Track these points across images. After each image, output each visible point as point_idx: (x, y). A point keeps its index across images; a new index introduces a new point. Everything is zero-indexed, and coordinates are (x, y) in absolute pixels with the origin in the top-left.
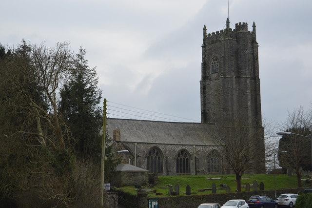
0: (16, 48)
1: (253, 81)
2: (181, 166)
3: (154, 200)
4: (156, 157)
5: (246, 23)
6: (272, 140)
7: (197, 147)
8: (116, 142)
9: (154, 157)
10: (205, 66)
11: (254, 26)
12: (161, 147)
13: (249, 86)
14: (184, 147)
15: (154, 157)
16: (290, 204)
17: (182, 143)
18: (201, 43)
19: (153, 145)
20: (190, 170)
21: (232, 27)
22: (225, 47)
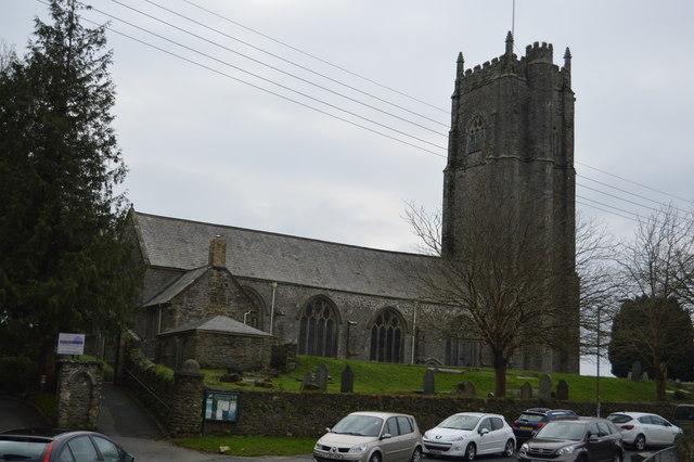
1: (560, 173)
2: (382, 345)
3: (226, 395)
4: (322, 321)
5: (551, 45)
6: (612, 376)
8: (214, 268)
10: (456, 137)
11: (568, 56)
12: (335, 298)
13: (550, 179)
14: (392, 303)
16: (637, 441)
17: (387, 294)
18: (451, 90)
19: (319, 292)
20: (403, 357)
21: (520, 52)
22: (502, 93)
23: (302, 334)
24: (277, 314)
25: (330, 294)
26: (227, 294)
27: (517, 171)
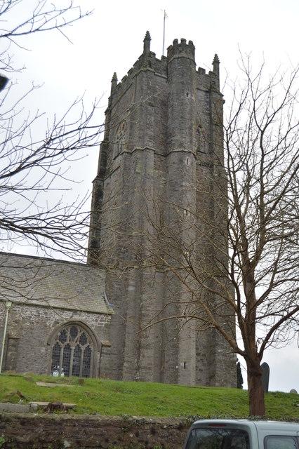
5: (191, 42)
7: (18, 309)
11: (216, 62)
21: (159, 50)
27: (152, 163)
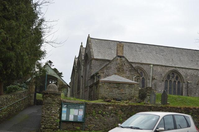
0: (42, 11)
8: (118, 56)
9: (173, 81)
12: (180, 71)
15: (173, 81)
23: (166, 88)
24: (153, 79)
25: (178, 69)
26: (125, 68)
